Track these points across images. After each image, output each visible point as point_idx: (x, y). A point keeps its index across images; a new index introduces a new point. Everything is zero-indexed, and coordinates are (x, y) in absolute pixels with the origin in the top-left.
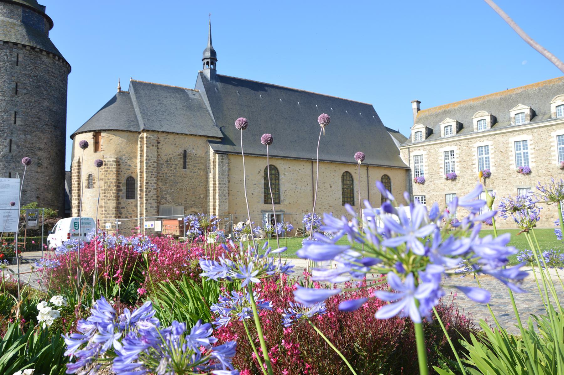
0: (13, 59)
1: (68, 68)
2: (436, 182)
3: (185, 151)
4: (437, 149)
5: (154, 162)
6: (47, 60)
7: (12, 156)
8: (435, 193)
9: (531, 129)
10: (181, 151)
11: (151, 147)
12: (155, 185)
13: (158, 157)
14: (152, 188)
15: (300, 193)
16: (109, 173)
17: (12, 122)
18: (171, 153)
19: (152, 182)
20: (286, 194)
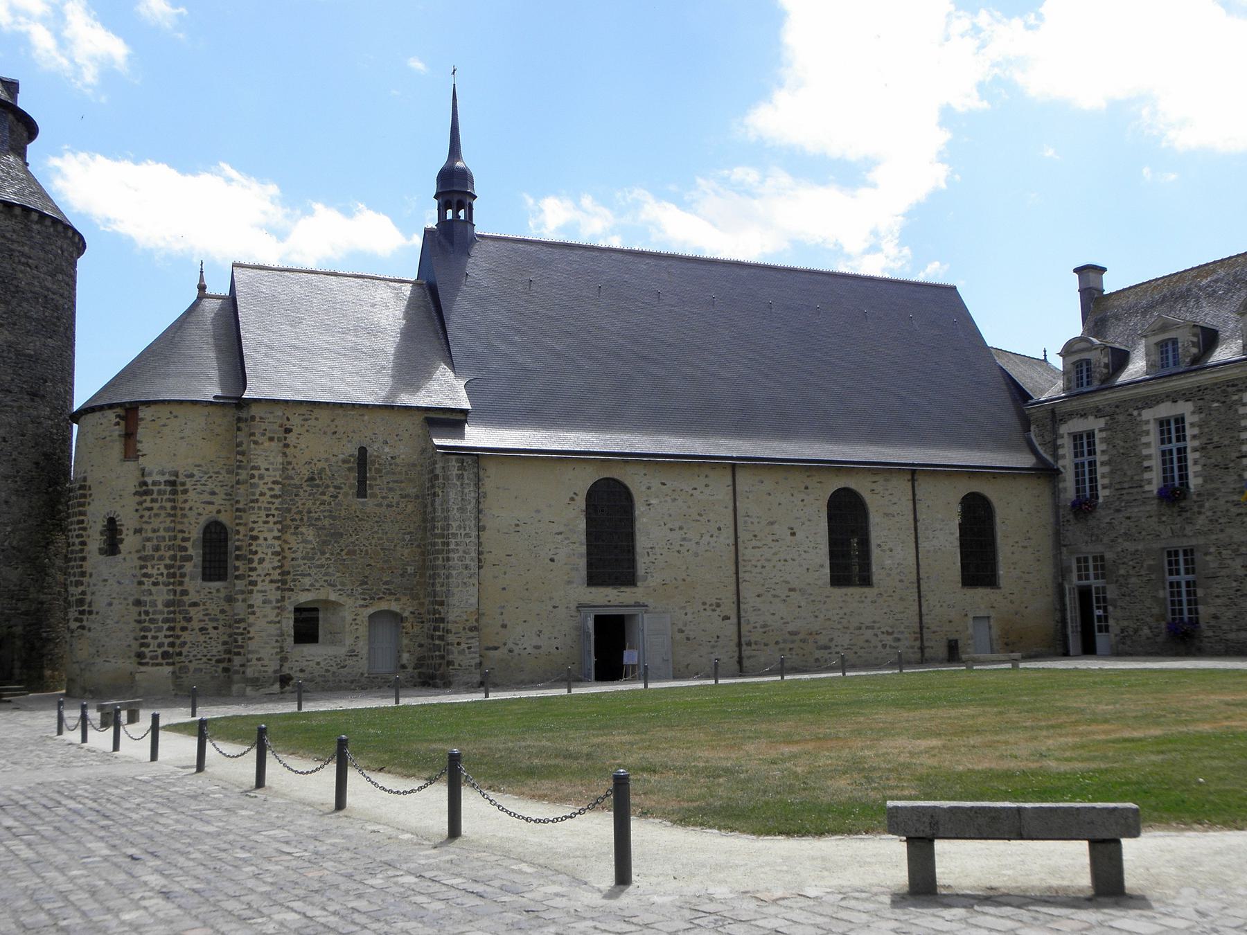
1: (72, 239)
2: (1134, 511)
3: (363, 451)
4: (1135, 413)
5: (274, 482)
6: (7, 223)
8: (1130, 546)
9: (734, 465)
10: (351, 449)
11: (267, 444)
12: (277, 543)
13: (284, 469)
14: (270, 551)
15: (696, 555)
16: (156, 515)
18: (326, 456)
19: (269, 536)
20: (652, 558)
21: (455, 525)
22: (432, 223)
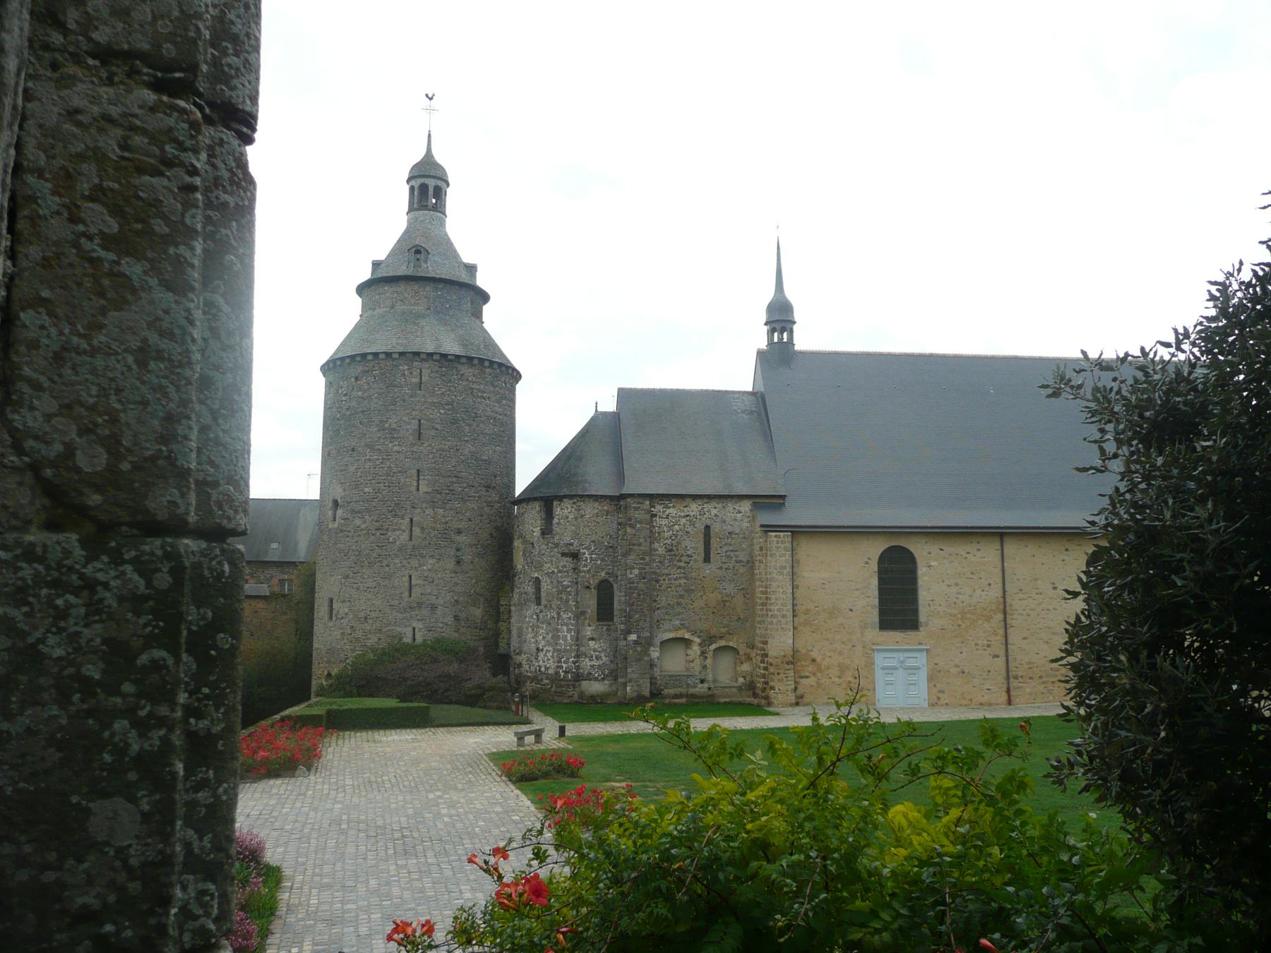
0: (414, 380)
3: (707, 528)
7: (414, 547)
9: (1001, 535)
17: (413, 489)
21: (774, 584)
22: (763, 344)
